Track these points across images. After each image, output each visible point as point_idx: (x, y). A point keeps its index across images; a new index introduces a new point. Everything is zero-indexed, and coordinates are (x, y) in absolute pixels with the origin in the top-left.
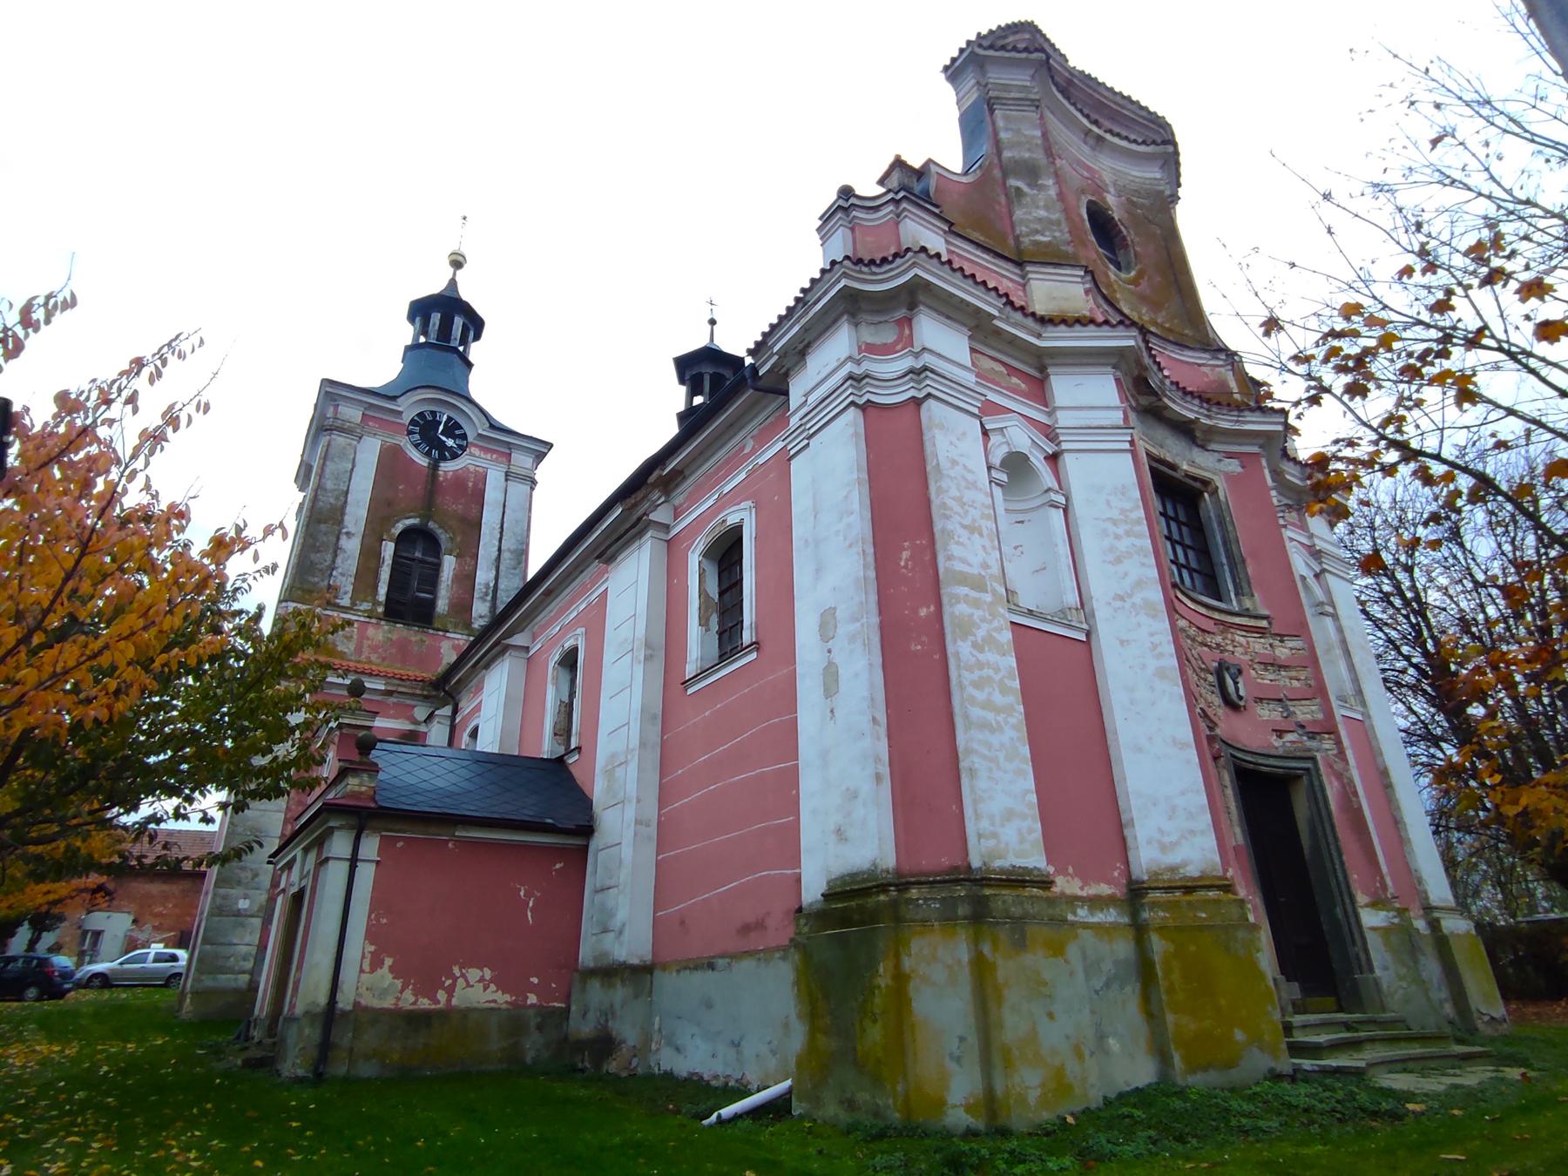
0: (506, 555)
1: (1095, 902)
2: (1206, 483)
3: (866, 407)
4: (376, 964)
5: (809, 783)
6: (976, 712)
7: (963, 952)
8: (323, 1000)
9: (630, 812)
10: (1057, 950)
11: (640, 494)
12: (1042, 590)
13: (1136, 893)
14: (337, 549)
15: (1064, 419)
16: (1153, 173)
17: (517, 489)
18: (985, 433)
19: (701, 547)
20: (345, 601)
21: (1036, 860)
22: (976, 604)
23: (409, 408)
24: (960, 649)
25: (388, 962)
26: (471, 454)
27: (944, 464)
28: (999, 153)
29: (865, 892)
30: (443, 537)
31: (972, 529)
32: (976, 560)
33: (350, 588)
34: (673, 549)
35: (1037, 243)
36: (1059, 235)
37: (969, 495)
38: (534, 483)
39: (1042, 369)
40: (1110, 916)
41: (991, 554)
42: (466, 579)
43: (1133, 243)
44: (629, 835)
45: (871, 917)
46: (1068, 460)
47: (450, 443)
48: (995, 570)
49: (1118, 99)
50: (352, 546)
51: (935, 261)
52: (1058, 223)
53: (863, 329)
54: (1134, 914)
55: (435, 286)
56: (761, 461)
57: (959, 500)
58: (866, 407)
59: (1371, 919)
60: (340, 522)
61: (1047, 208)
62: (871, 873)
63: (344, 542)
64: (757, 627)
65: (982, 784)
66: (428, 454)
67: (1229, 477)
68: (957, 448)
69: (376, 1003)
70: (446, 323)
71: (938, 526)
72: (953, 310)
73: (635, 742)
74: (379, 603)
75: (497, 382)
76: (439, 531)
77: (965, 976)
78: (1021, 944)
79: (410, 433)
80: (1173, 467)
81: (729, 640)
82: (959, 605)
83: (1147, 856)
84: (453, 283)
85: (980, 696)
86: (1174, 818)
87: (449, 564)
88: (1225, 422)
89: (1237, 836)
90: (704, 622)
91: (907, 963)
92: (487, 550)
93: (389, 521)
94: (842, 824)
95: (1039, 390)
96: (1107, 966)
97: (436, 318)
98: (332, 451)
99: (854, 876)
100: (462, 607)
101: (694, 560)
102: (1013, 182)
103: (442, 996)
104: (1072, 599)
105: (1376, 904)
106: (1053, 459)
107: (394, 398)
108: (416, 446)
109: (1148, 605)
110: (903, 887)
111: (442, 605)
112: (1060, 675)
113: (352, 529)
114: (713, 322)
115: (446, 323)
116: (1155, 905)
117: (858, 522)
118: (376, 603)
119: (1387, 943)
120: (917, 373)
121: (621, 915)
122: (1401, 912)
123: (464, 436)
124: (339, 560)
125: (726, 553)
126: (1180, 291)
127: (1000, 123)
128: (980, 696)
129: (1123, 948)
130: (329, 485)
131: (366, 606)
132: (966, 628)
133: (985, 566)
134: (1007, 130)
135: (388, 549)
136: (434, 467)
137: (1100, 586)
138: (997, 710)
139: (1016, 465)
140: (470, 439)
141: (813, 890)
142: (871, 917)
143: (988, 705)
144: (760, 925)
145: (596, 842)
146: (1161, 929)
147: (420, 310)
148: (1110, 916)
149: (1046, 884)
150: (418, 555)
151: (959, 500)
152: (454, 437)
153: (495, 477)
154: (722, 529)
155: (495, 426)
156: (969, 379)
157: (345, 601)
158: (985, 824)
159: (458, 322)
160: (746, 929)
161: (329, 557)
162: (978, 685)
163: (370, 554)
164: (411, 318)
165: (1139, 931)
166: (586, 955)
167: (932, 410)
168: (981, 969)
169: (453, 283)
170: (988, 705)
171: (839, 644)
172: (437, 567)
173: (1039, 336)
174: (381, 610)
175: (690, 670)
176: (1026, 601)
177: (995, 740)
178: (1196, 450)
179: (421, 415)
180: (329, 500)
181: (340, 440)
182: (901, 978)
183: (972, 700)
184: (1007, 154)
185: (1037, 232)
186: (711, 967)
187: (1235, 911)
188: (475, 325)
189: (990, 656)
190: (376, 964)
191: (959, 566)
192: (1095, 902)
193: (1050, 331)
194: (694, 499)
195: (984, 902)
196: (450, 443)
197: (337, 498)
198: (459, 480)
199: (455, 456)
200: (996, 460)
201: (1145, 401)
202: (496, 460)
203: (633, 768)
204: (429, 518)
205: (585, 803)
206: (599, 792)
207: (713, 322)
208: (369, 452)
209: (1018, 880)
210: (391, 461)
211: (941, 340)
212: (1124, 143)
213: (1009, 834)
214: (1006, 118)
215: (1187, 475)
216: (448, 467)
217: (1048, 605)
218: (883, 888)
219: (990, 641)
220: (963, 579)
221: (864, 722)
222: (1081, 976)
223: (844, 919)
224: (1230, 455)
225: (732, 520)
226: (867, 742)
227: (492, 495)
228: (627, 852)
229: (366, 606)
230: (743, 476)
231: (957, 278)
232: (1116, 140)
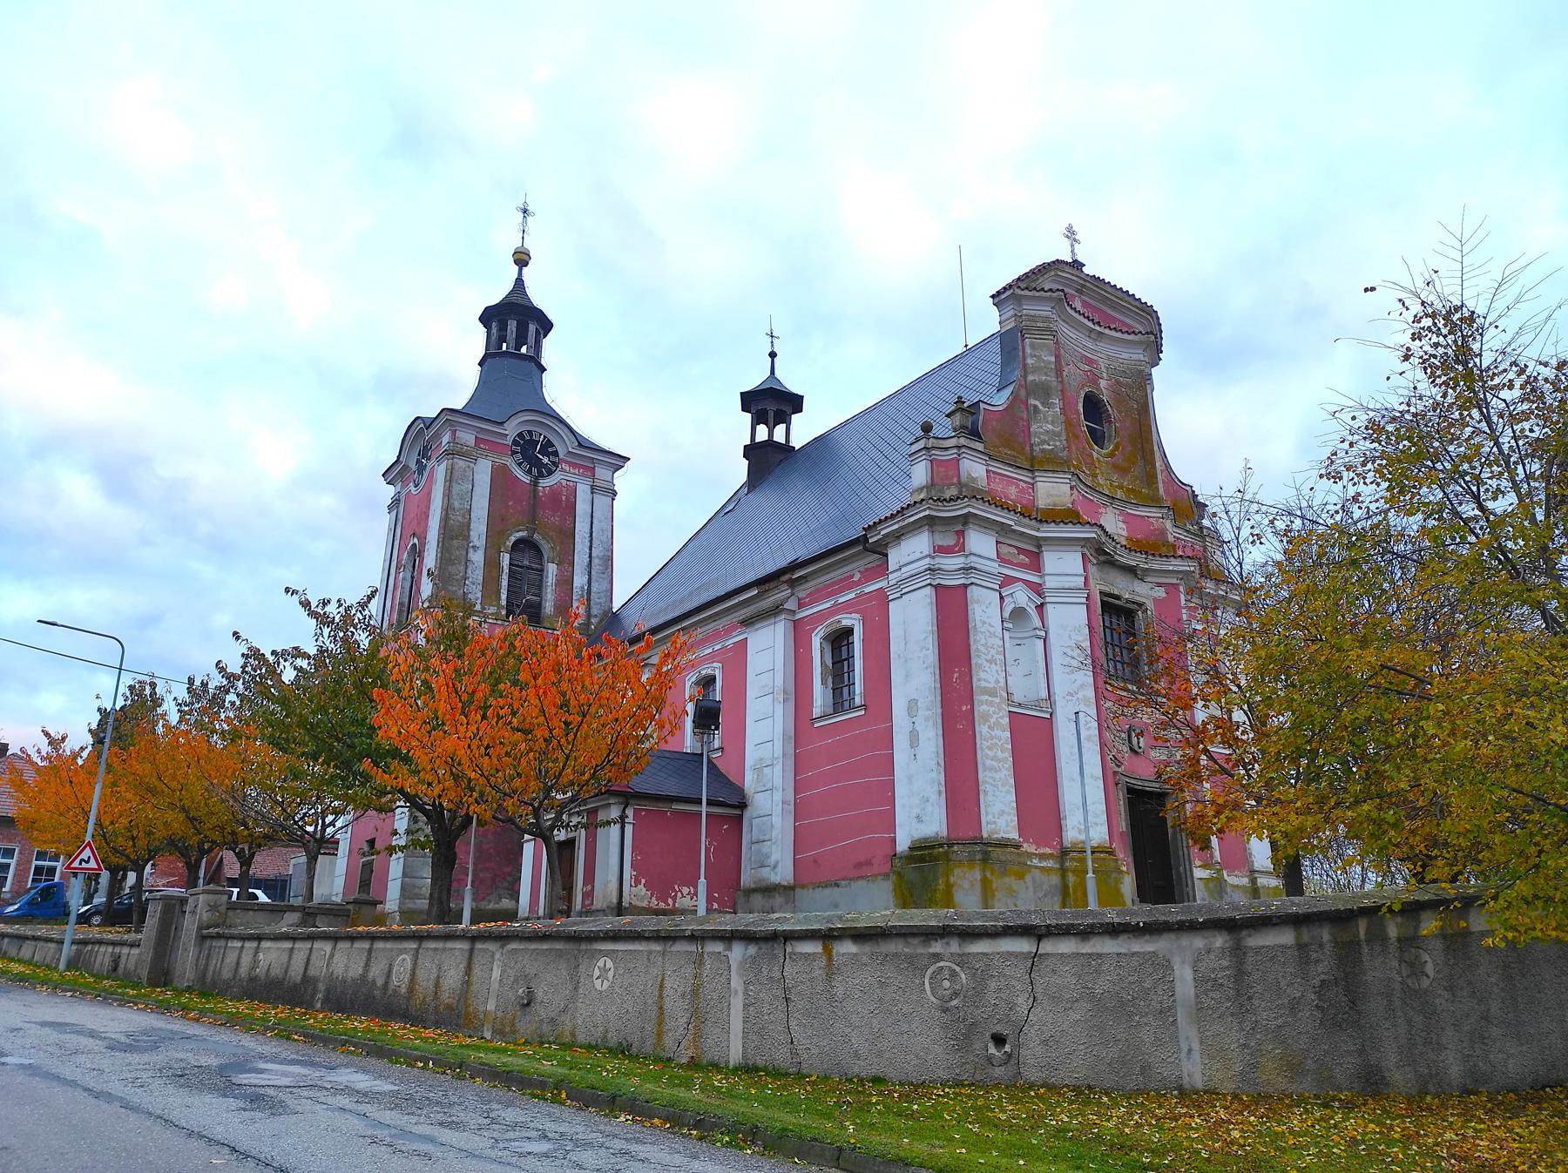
0: (596, 561)
1: (1042, 857)
2: (1141, 605)
3: (937, 587)
4: (637, 882)
5: (900, 790)
6: (988, 762)
7: (978, 875)
8: (615, 901)
9: (778, 796)
10: (1021, 876)
11: (772, 585)
12: (1027, 688)
13: (1064, 853)
15: (1050, 582)
16: (1138, 355)
17: (601, 501)
18: (1002, 598)
19: (822, 634)
21: (1014, 835)
22: (991, 704)
24: (982, 729)
26: (563, 470)
27: (979, 624)
28: (1025, 377)
29: (932, 847)
30: (546, 547)
31: (991, 661)
32: (992, 680)
34: (800, 634)
35: (1043, 451)
36: (1056, 444)
37: (991, 641)
38: (615, 493)
39: (1039, 547)
40: (1050, 863)
41: (1004, 670)
42: (566, 582)
43: (1116, 424)
44: (777, 810)
45: (935, 859)
46: (1049, 608)
47: (546, 460)
48: (1002, 684)
49: (1119, 294)
50: (478, 557)
52: (1058, 435)
53: (937, 536)
54: (1062, 863)
56: (867, 590)
57: (985, 645)
58: (937, 587)
59: (1199, 873)
60: (467, 538)
61: (1053, 423)
62: (936, 838)
64: (865, 695)
65: (990, 798)
66: (529, 472)
67: (1156, 600)
68: (985, 610)
69: (639, 904)
70: (515, 326)
71: (973, 662)
72: (986, 524)
73: (779, 752)
75: (575, 388)
77: (978, 886)
78: (1003, 874)
79: (514, 453)
80: (1118, 598)
81: (840, 700)
82: (983, 705)
83: (1073, 832)
84: (519, 282)
85: (991, 754)
86: (1087, 813)
87: (552, 570)
88: (1156, 565)
89: (1123, 825)
90: (824, 682)
91: (952, 880)
92: (580, 559)
94: (918, 813)
95: (1035, 564)
96: (1045, 887)
97: (512, 325)
98: (457, 474)
99: (925, 839)
100: (563, 607)
101: (816, 642)
102: (1033, 402)
103: (670, 901)
104: (1044, 694)
105: (1204, 867)
106: (1040, 608)
108: (519, 465)
109: (1086, 699)
110: (950, 845)
111: (548, 607)
112: (1033, 739)
113: (476, 543)
114: (773, 355)
115: (515, 326)
116: (1072, 859)
117: (930, 655)
118: (499, 607)
119: (1206, 886)
120: (967, 569)
121: (774, 857)
122: (1218, 871)
123: (556, 454)
125: (840, 639)
126: (1144, 457)
127: (1028, 351)
128: (991, 754)
129: (1055, 879)
130: (456, 505)
131: (492, 610)
132: (985, 718)
133: (997, 681)
134: (1032, 356)
135: (506, 559)
136: (536, 484)
137: (1059, 690)
138: (999, 761)
139: (1019, 614)
141: (903, 845)
142: (935, 859)
143: (994, 758)
144: (869, 863)
145: (747, 814)
146: (1074, 871)
147: (487, 317)
148: (1050, 863)
149: (1018, 847)
150: (526, 562)
151: (985, 645)
152: (548, 455)
153: (583, 491)
154: (834, 627)
155: (583, 443)
156: (994, 567)
158: (990, 817)
159: (532, 328)
160: (859, 865)
162: (990, 748)
163: (492, 564)
165: (1063, 871)
166: (746, 879)
167: (973, 592)
168: (985, 882)
169: (519, 282)
170: (994, 758)
171: (919, 720)
172: (541, 571)
173: (1038, 530)
175: (817, 712)
176: (1017, 698)
177: (997, 776)
178: (1137, 582)
179: (520, 435)
180: (456, 518)
181: (461, 463)
182: (949, 886)
183: (987, 756)
184: (1030, 378)
185: (1044, 442)
186: (837, 885)
187: (1112, 864)
188: (546, 326)
189: (998, 733)
190: (637, 882)
191: (983, 684)
192: (1042, 857)
193: (1045, 527)
194: (816, 597)
195: (988, 852)
196: (546, 460)
198: (555, 493)
199: (550, 473)
200: (1006, 615)
201: (1102, 558)
202: (583, 475)
203: (778, 769)
204: (534, 530)
205: (739, 791)
206: (749, 782)
207: (773, 355)
208: (483, 471)
209: (1004, 844)
210: (500, 478)
211: (981, 544)
212: (1119, 335)
213: (1001, 822)
214: (1033, 346)
215: (1128, 601)
216: (545, 483)
217: (1032, 696)
218: (941, 845)
219: (997, 723)
220: (986, 691)
221: (933, 764)
222: (1031, 890)
223: (922, 859)
224: (1159, 585)
225: (846, 623)
226: (934, 774)
227: (582, 507)
228: (777, 820)
229: (492, 610)
230: (852, 596)
231: (992, 509)
232: (1113, 333)
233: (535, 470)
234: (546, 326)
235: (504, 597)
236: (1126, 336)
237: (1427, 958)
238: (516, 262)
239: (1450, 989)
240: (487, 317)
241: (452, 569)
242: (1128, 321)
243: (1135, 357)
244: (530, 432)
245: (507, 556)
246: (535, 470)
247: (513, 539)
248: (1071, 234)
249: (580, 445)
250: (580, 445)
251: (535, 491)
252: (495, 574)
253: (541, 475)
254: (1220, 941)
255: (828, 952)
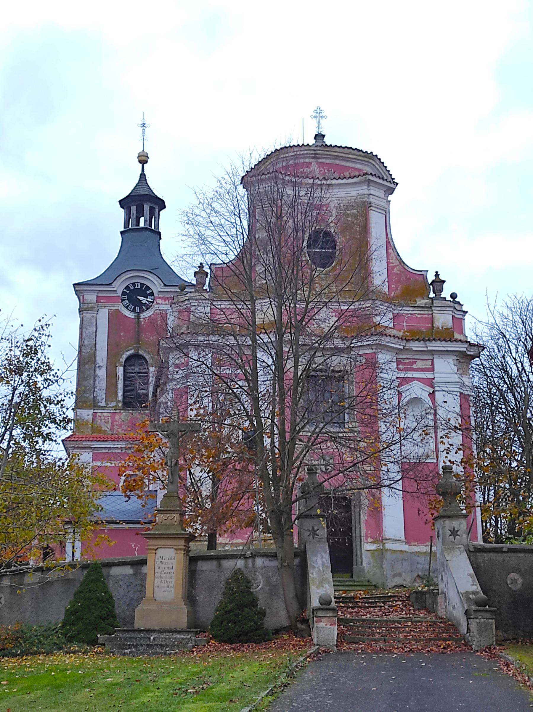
14: (95, 376)
20: (103, 404)
23: (119, 287)
25: (441, 329)
33: (104, 396)
50: (102, 373)
51: (382, 164)
55: (126, 189)
60: (95, 362)
63: (98, 372)
66: (134, 311)
74: (120, 401)
76: (144, 355)
79: (123, 300)
84: (143, 176)
90: (359, 195)
93: (118, 355)
97: (134, 209)
107: (110, 284)
108: (127, 307)
123: (152, 294)
124: (97, 382)
131: (113, 404)
135: (120, 371)
136: (139, 317)
140: (156, 294)
147: (123, 203)
150: (137, 369)
157: (103, 404)
159: (146, 208)
161: (92, 382)
163: (111, 375)
164: (122, 207)
169: (143, 176)
174: (120, 405)
179: (127, 287)
180: (87, 350)
197: (91, 349)
198: (151, 320)
204: (138, 348)
210: (115, 318)
229: (113, 404)
233: (137, 309)
234: (162, 205)
235: (120, 394)
236: (350, 181)
237: (2, 596)
238: (140, 162)
239: (10, 608)
240: (123, 203)
241: (85, 383)
242: (359, 166)
243: (361, 192)
244: (134, 284)
245: (121, 369)
246: (137, 309)
247: (125, 357)
248: (319, 114)
249: (165, 285)
250: (165, 285)
251: (139, 322)
252: (114, 381)
253: (142, 311)
254: (215, 563)
255: (220, 566)
